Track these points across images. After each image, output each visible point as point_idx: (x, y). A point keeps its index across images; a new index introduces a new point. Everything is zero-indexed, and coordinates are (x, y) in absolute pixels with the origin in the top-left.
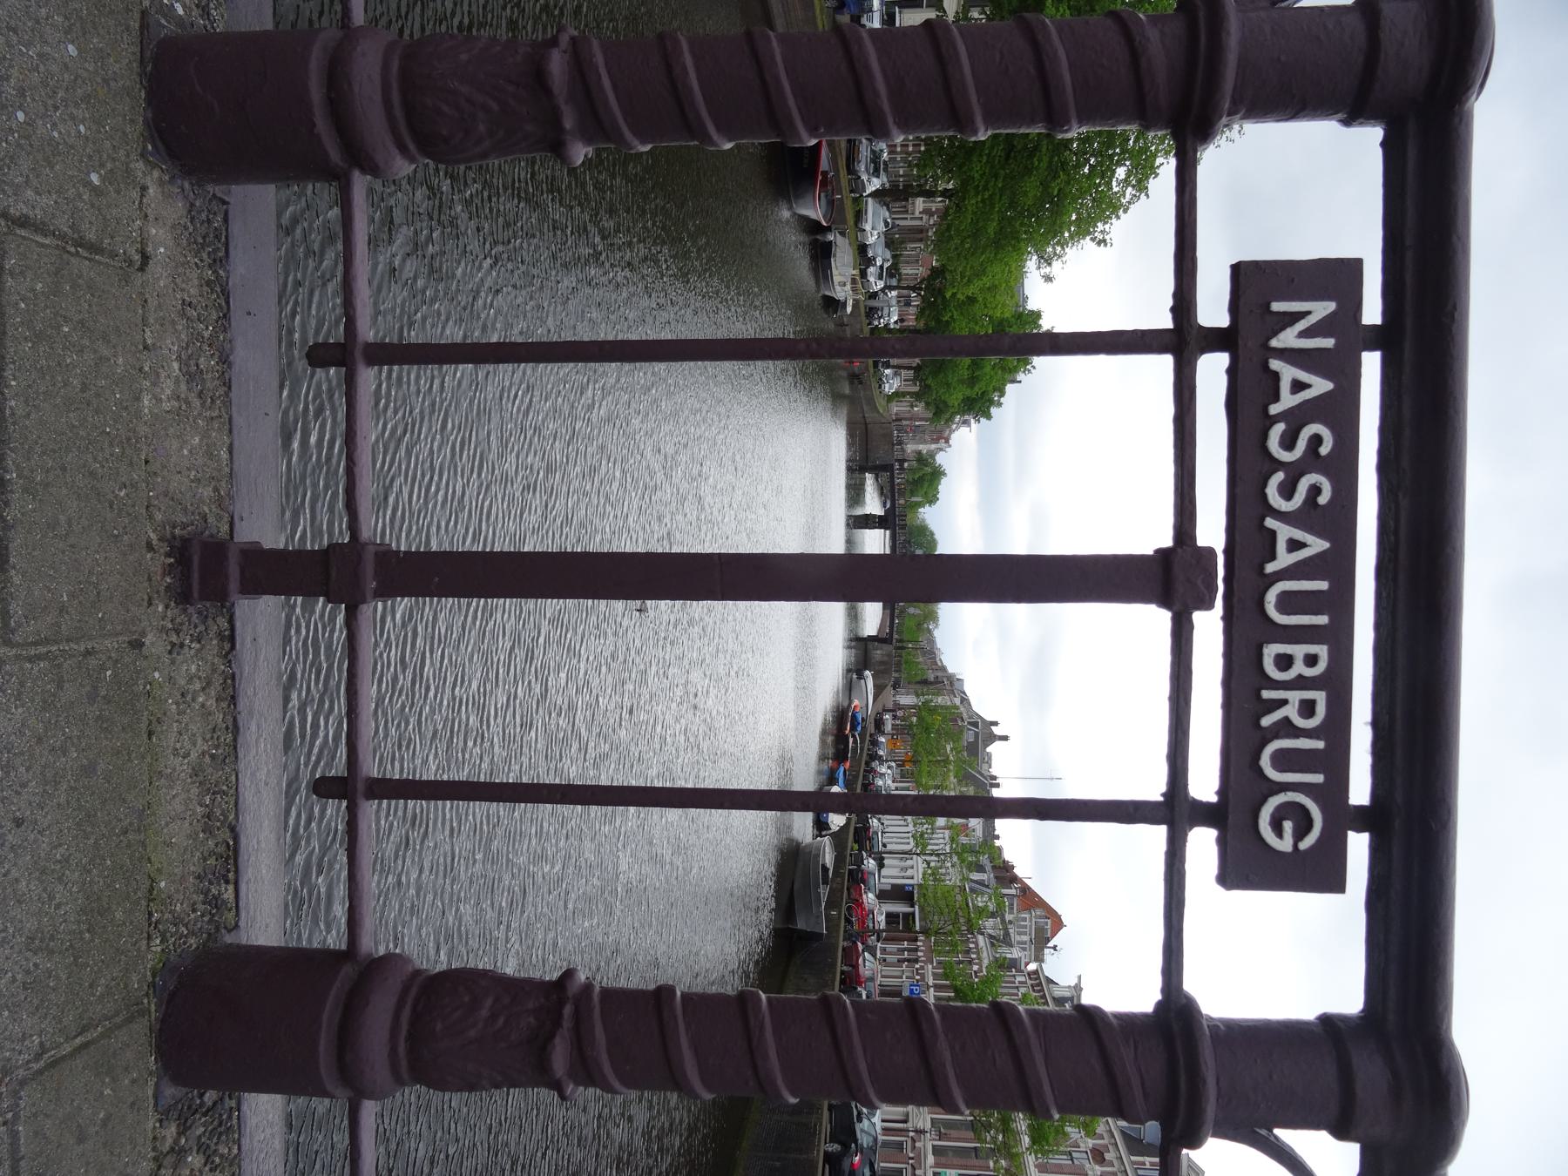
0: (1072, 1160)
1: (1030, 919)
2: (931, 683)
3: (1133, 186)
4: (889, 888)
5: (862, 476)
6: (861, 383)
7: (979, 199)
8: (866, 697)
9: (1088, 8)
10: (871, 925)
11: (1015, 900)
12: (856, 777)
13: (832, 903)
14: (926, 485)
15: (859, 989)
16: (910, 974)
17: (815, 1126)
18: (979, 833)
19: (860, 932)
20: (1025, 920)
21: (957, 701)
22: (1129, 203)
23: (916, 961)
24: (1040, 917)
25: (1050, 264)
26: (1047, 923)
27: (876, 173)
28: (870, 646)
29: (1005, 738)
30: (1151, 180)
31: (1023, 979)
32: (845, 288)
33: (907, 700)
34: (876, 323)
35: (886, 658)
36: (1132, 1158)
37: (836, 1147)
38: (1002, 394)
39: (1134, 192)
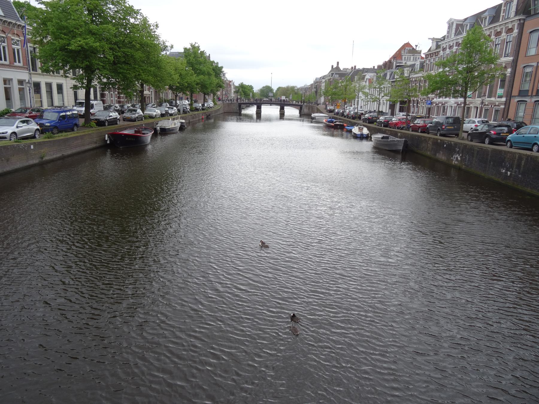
0: (499, 44)
1: (405, 55)
2: (317, 90)
3: (137, 15)
4: (390, 110)
5: (242, 115)
6: (210, 115)
7: (143, 74)
8: (322, 116)
9: (72, 33)
10: (404, 120)
11: (397, 61)
12: (350, 122)
13: (395, 135)
14: (246, 90)
15: (428, 126)
16: (422, 103)
17: (478, 148)
18: (372, 74)
19: (406, 124)
20: (405, 58)
21: (324, 80)
22: (143, 17)
23: (418, 101)
24: (405, 51)
25: (167, 46)
26: (407, 49)
27: (135, 111)
28: (302, 113)
29: (338, 63)
30: (134, 8)
31: (428, 61)
32: (176, 123)
33: (322, 100)
34: (188, 110)
35: (307, 108)
36: (501, 20)
37: (487, 140)
38: (213, 62)
39: (139, 15)
